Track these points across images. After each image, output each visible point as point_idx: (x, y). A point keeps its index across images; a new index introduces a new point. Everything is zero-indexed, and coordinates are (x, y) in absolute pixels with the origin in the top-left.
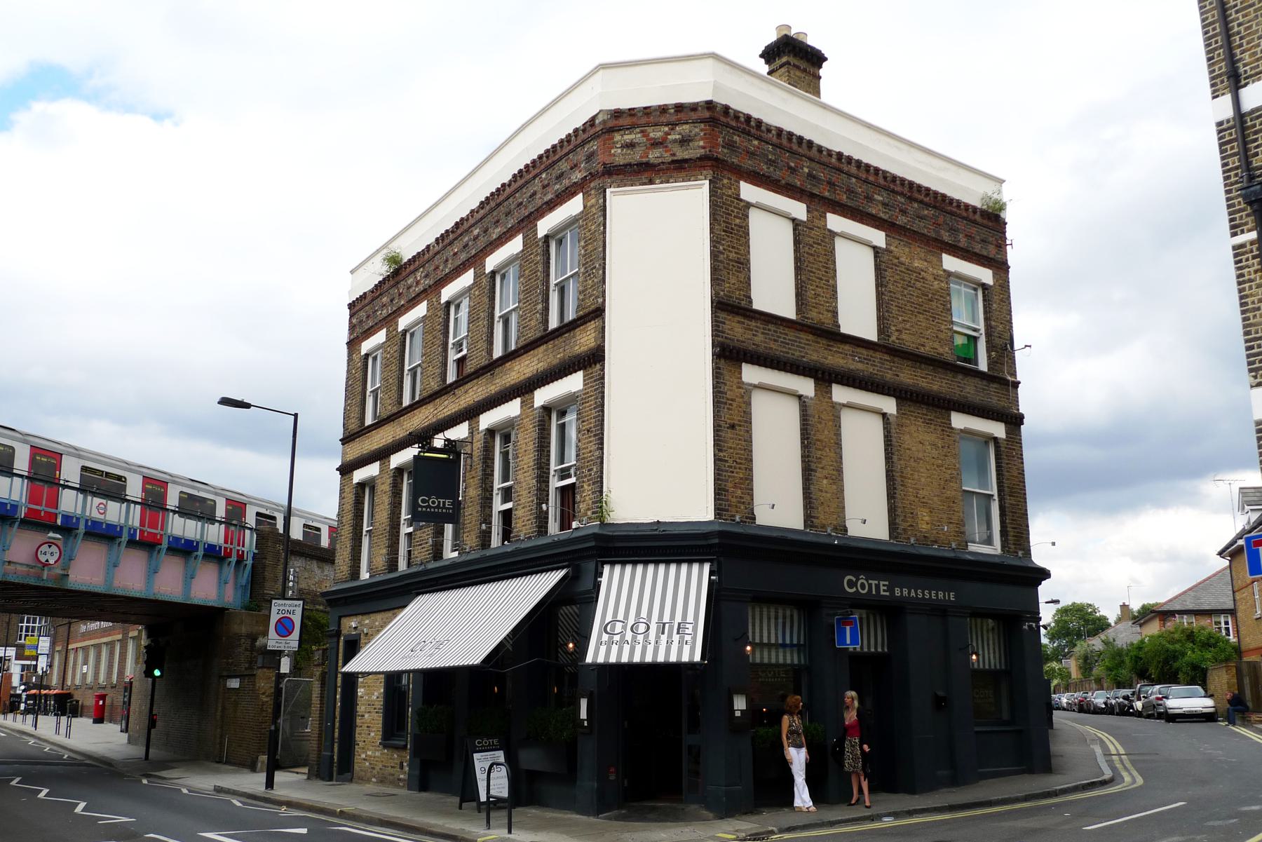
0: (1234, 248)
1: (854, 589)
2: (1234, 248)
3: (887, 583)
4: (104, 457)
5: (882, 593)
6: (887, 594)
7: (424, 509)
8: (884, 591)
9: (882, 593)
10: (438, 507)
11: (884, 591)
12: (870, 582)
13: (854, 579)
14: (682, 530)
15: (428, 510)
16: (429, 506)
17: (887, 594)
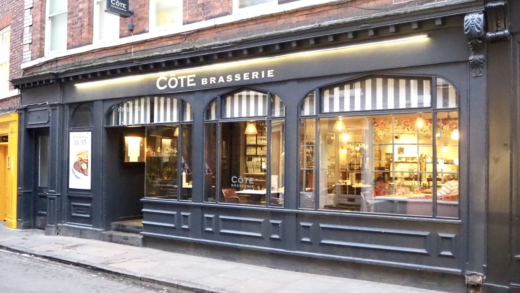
0: (7, 141)
1: (166, 86)
2: (7, 141)
3: (273, 71)
4: (279, 183)
5: (189, 85)
6: (194, 84)
7: (235, 185)
8: (191, 83)
9: (189, 85)
10: (119, 7)
11: (191, 83)
12: (245, 178)
13: (236, 178)
14: (178, 117)
15: (238, 186)
16: (115, 5)
17: (194, 84)
